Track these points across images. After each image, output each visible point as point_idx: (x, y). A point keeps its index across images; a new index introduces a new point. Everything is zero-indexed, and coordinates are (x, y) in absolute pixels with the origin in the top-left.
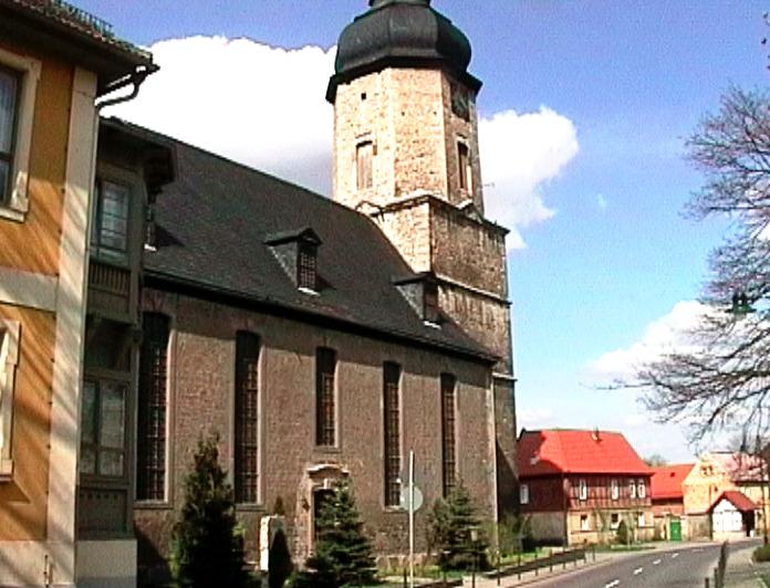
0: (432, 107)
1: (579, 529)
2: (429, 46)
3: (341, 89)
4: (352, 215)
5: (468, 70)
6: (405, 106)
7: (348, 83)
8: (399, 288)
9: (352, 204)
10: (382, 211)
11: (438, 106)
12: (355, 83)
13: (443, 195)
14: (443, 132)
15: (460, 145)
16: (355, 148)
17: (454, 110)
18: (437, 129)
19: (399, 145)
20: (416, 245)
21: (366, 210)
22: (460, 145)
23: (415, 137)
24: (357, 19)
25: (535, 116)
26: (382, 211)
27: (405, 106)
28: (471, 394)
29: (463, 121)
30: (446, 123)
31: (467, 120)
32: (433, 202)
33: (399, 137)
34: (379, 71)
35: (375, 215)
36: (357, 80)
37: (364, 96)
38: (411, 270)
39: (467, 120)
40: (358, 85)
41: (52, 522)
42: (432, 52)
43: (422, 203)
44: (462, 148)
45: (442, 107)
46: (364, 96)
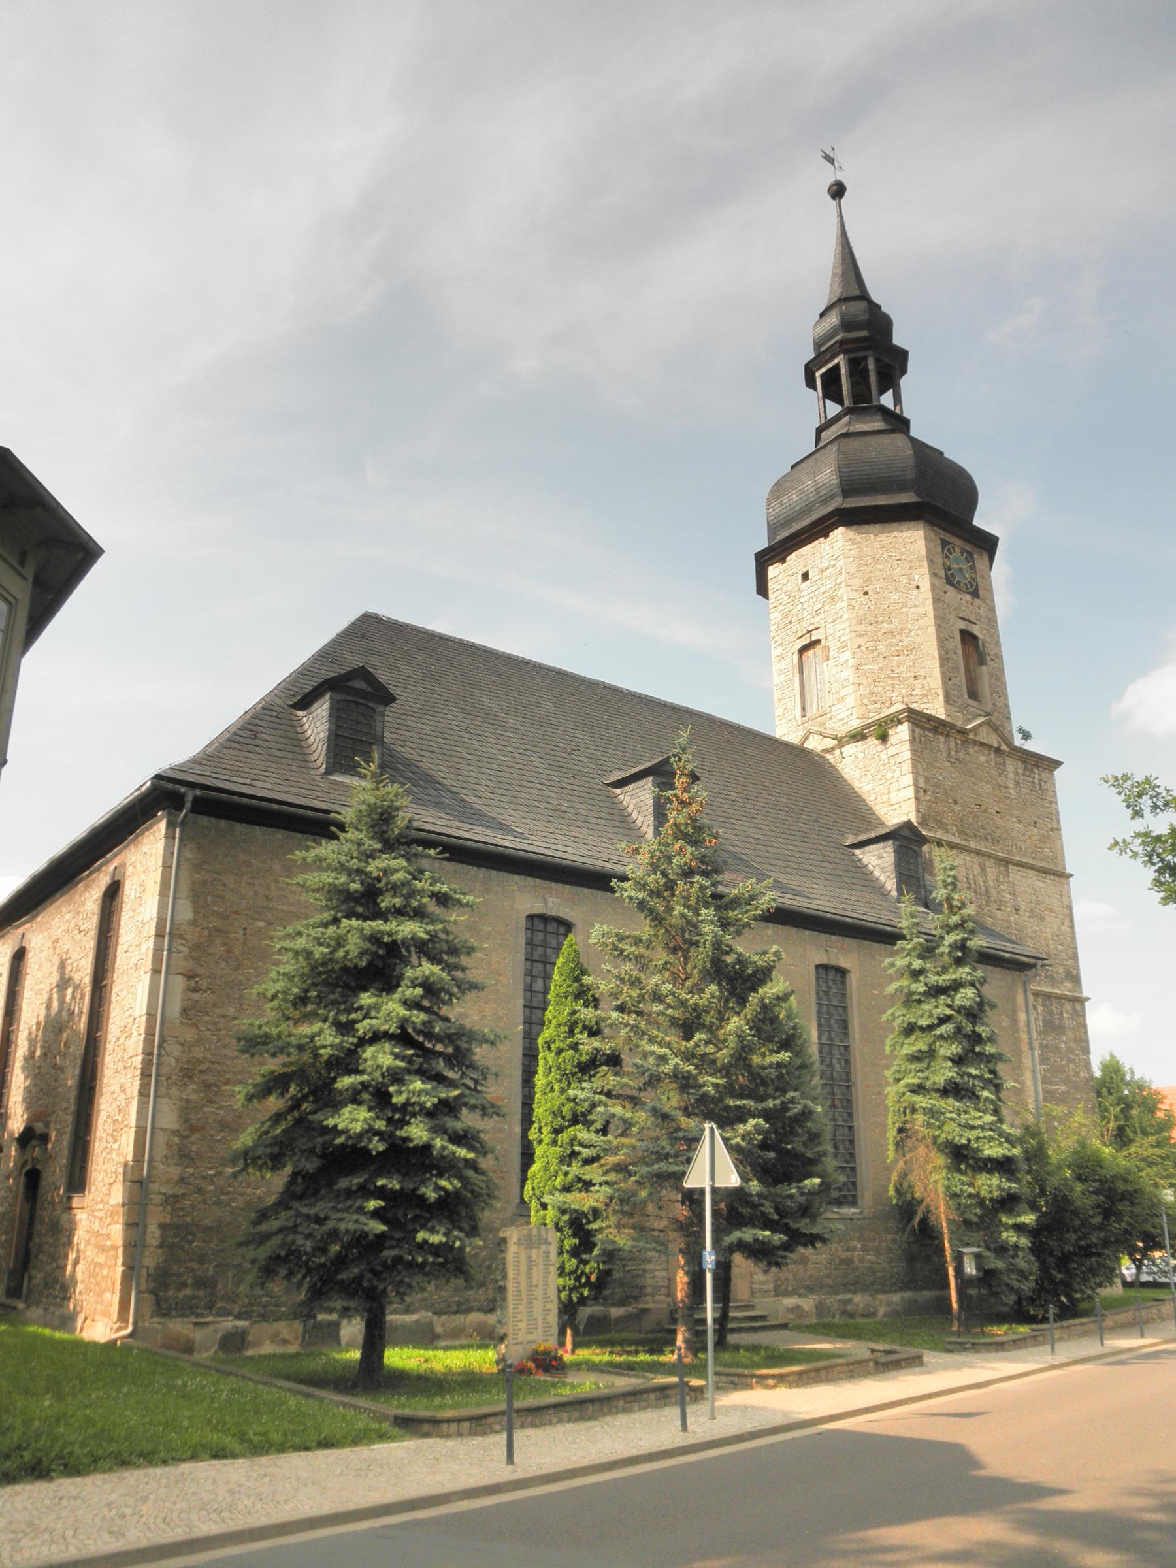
0: (911, 579)
1: (535, 964)
2: (902, 487)
3: (773, 571)
4: (798, 753)
5: (975, 523)
6: (868, 581)
7: (783, 561)
8: (857, 852)
9: (794, 738)
10: (841, 742)
11: (923, 577)
12: (792, 558)
13: (938, 709)
14: (931, 616)
15: (964, 633)
16: (796, 656)
17: (949, 582)
18: (921, 610)
19: (861, 641)
20: (893, 787)
21: (815, 744)
22: (964, 633)
23: (886, 626)
24: (793, 467)
25: (1127, 1062)
26: (841, 742)
27: (868, 581)
28: (926, 615)
29: (968, 597)
30: (937, 601)
31: (975, 594)
32: (918, 719)
33: (861, 628)
34: (826, 536)
35: (831, 750)
36: (793, 555)
37: (805, 576)
38: (883, 824)
39: (975, 594)
40: (797, 560)
41: (194, 761)
42: (907, 498)
43: (900, 722)
44: (968, 638)
45: (927, 577)
46: (805, 576)
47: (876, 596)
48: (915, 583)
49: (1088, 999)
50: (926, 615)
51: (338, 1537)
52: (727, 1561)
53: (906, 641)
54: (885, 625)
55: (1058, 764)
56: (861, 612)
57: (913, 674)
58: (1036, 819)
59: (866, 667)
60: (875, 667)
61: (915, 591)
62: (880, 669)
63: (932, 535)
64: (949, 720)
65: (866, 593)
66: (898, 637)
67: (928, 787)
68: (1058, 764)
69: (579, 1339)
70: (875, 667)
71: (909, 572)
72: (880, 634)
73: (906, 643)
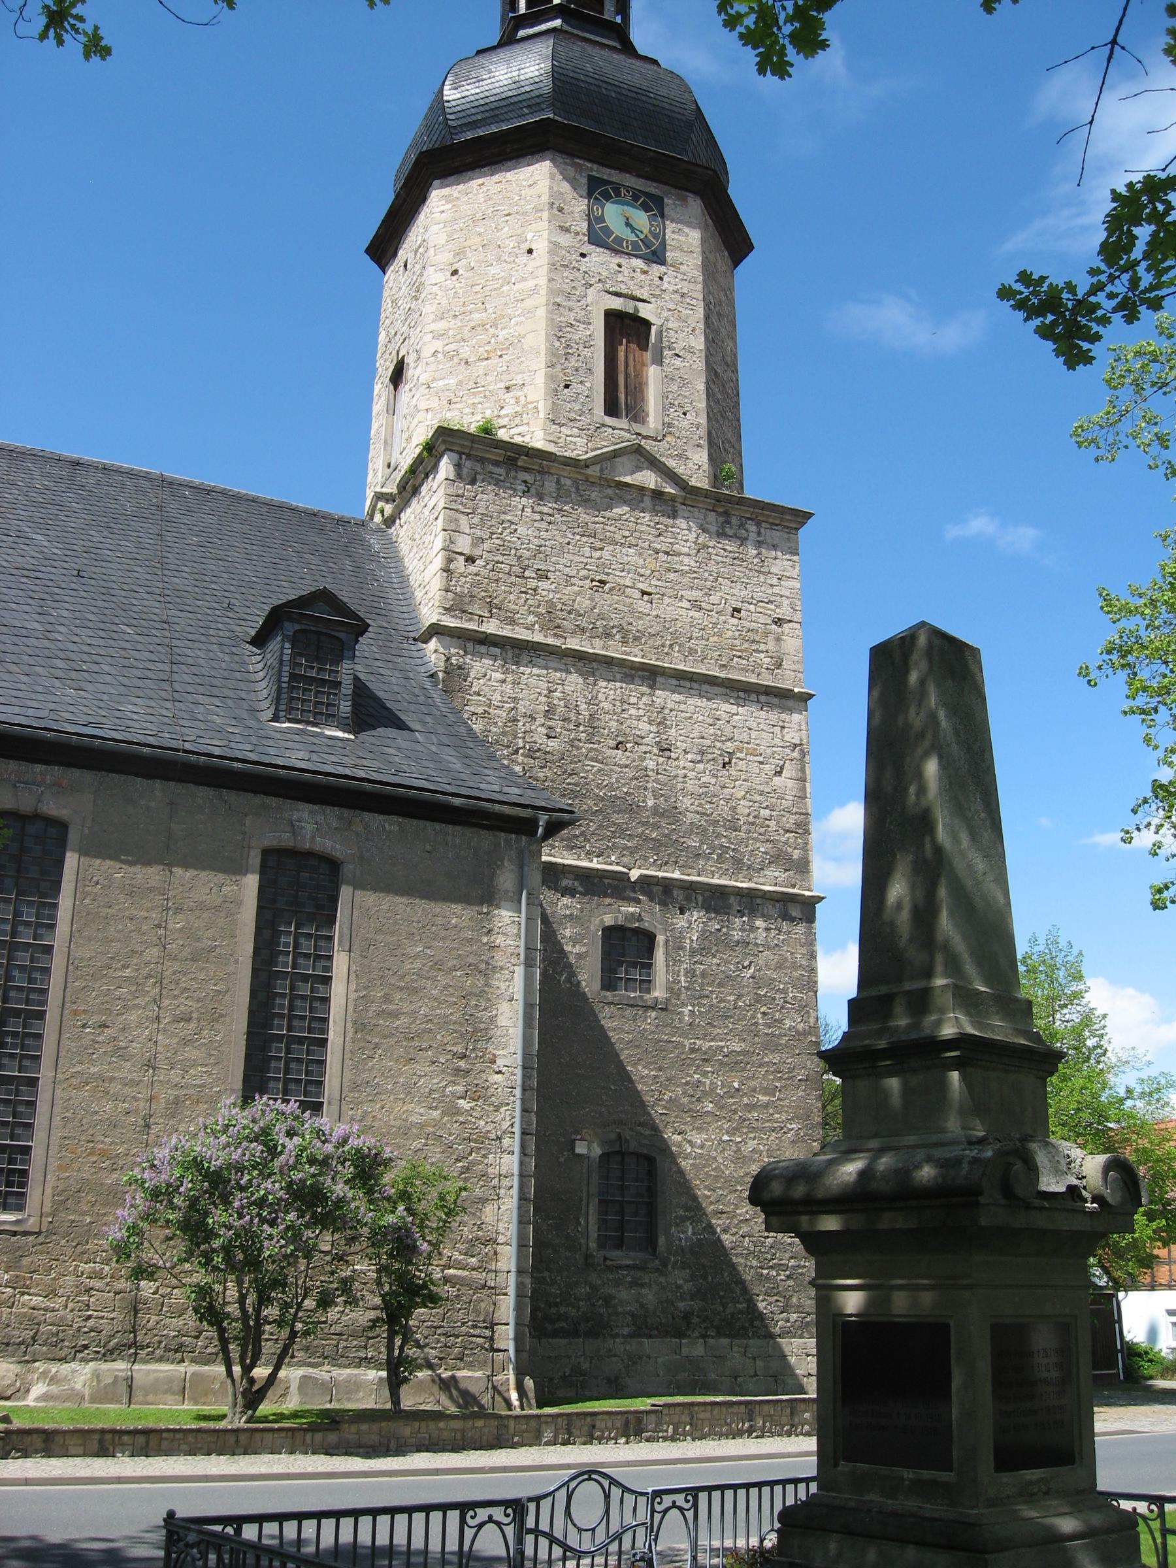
6: (460, 254)
47: (470, 274)
48: (526, 246)
49: (820, 899)
50: (534, 291)
51: (118, 1489)
52: (55, 1565)
53: (502, 334)
54: (476, 316)
55: (802, 517)
56: (444, 302)
57: (503, 385)
58: (738, 605)
59: (441, 383)
60: (452, 381)
61: (525, 258)
62: (460, 383)
63: (571, 171)
64: (551, 448)
65: (455, 272)
66: (492, 331)
67: (477, 552)
68: (802, 517)
69: (780, 1390)
70: (452, 381)
71: (519, 231)
72: (466, 330)
73: (501, 338)
